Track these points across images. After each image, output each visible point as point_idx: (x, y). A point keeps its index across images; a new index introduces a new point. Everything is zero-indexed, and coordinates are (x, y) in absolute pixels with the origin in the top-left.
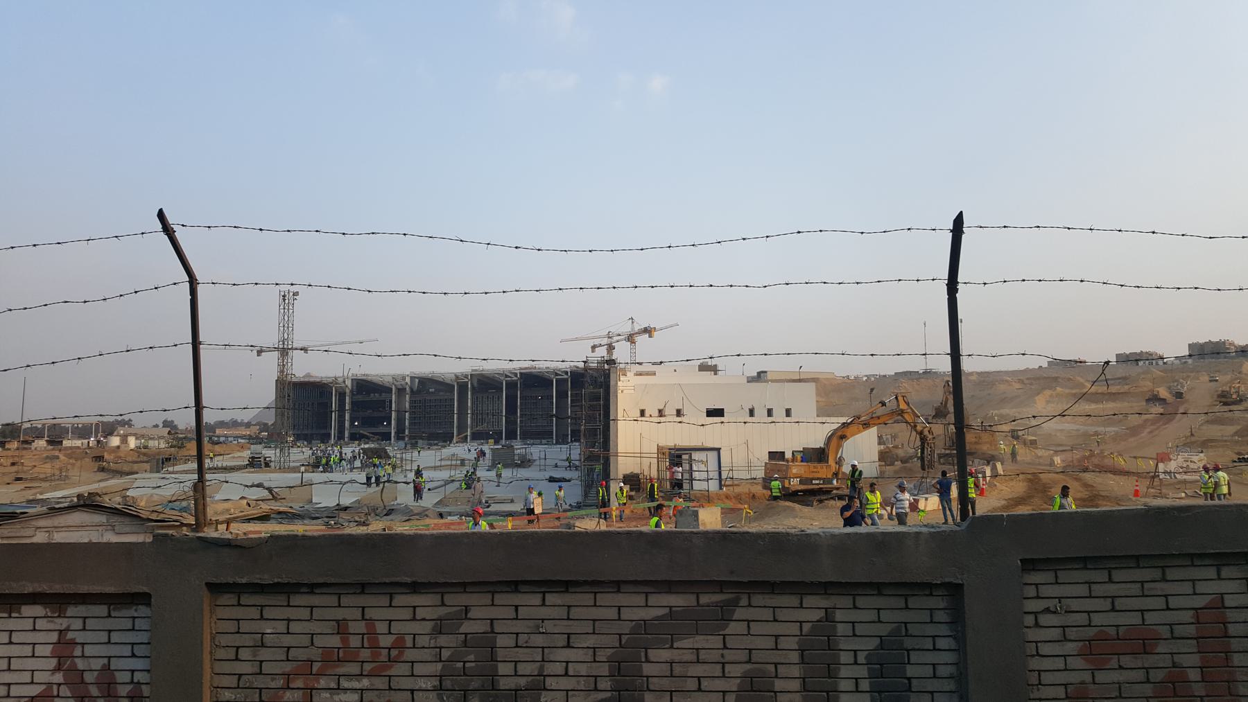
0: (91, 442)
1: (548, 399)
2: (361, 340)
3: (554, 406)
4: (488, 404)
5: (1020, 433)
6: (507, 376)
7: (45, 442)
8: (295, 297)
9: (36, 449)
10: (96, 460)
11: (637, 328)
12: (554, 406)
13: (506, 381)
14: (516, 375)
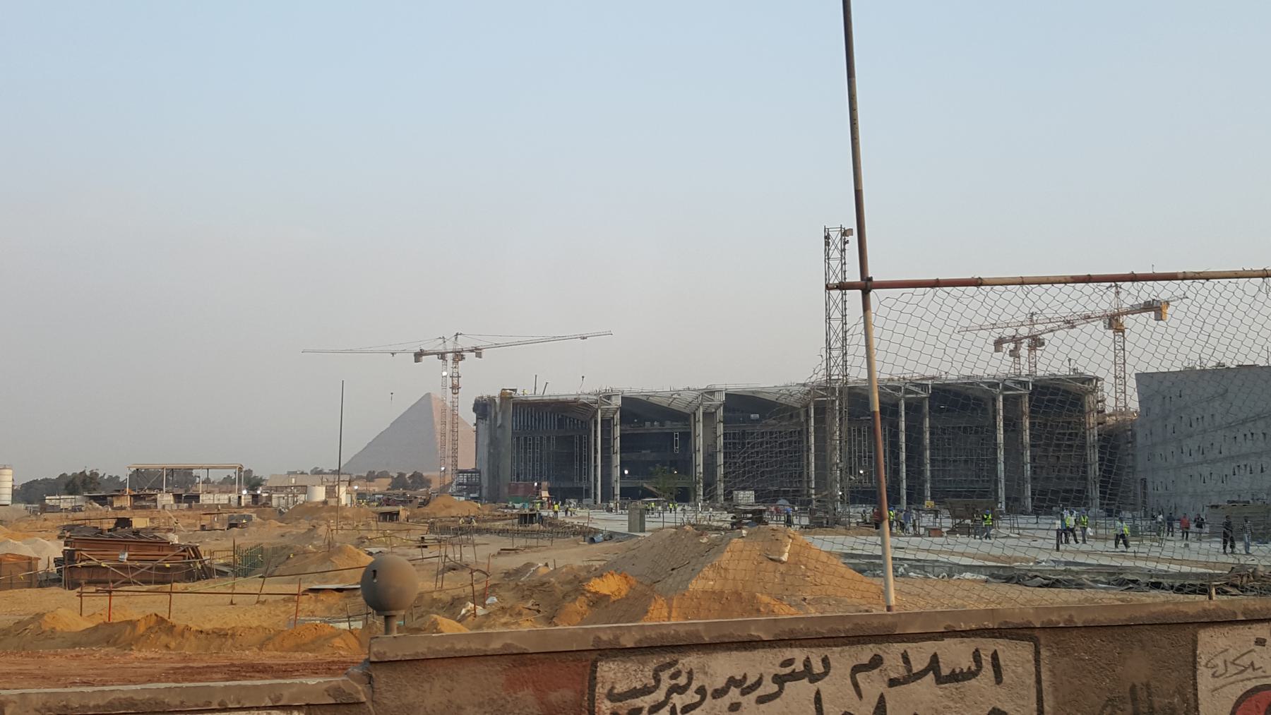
0: (243, 497)
1: (976, 432)
2: (584, 333)
5: (1104, 514)
6: (908, 391)
7: (172, 498)
9: (164, 507)
10: (385, 520)
14: (924, 387)
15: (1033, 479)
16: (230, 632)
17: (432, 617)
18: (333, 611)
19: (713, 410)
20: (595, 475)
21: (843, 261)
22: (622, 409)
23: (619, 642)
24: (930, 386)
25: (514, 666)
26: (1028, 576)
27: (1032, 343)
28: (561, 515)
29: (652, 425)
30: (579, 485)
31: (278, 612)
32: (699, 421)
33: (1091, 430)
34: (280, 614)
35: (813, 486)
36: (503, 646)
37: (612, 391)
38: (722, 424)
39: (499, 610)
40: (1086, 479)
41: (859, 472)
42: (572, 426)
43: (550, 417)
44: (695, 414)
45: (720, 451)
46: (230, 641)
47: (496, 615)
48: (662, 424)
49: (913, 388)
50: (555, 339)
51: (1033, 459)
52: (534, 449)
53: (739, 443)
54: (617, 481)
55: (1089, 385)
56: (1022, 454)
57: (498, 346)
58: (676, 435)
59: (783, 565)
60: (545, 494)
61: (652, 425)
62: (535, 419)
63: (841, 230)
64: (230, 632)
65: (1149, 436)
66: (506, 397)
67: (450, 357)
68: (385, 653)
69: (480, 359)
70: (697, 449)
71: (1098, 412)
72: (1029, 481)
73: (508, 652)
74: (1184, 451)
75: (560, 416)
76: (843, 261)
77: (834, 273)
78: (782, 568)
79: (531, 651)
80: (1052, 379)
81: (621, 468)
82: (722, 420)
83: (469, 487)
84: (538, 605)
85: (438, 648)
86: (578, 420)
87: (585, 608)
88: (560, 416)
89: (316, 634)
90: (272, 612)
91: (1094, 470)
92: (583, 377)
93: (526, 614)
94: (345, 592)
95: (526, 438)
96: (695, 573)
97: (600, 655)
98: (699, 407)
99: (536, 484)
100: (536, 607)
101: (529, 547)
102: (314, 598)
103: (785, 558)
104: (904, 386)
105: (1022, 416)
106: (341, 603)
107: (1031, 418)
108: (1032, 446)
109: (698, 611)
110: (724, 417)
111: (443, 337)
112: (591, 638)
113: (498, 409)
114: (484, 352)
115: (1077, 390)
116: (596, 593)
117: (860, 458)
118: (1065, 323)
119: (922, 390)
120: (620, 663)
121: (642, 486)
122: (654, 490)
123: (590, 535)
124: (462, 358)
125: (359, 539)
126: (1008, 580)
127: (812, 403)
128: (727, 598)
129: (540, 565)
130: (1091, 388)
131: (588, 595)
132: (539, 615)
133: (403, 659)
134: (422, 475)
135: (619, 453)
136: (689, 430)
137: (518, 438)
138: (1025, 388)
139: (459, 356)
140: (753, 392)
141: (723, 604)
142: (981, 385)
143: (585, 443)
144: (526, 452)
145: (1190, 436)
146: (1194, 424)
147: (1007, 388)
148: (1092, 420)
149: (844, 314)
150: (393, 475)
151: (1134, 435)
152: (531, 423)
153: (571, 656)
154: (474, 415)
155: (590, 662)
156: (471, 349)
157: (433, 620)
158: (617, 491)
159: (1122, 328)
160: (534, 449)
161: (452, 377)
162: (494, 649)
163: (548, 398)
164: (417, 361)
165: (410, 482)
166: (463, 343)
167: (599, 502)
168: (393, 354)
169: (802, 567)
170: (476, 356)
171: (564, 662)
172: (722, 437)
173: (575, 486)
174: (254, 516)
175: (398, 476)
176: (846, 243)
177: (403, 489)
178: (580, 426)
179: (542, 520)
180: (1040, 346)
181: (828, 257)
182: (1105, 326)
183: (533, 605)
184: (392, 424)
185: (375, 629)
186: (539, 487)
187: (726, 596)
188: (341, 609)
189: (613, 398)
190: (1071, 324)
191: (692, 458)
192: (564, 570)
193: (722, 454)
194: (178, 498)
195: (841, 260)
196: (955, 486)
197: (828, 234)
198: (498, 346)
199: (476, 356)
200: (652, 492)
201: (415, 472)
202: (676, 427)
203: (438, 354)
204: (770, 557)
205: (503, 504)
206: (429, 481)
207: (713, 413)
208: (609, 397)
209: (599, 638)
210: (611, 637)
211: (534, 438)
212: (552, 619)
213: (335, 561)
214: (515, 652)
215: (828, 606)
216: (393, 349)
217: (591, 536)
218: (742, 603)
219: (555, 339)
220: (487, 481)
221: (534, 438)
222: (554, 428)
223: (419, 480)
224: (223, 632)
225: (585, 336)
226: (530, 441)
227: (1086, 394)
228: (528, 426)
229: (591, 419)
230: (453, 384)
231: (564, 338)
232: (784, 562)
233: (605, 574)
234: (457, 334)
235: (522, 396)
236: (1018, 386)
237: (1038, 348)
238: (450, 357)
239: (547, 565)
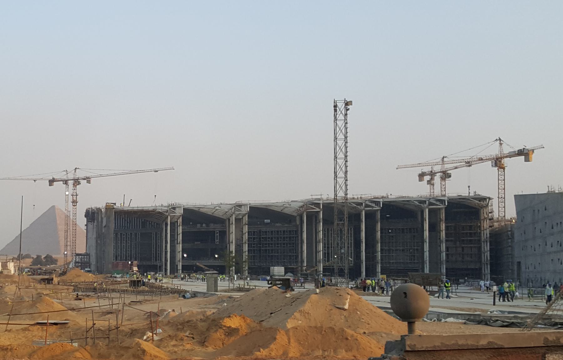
2: (156, 168)
6: (367, 206)
8: (348, 107)
11: (507, 150)
14: (377, 203)
15: (447, 261)
16: (9, 347)
17: (136, 340)
18: (54, 336)
19: (241, 217)
20: (166, 257)
21: (346, 122)
23: (560, 342)
24: (381, 203)
25: (494, 356)
26: (493, 321)
27: (443, 176)
28: (153, 281)
29: (201, 226)
30: (155, 263)
31: (20, 337)
32: (232, 223)
33: (485, 231)
34: (22, 338)
35: (305, 265)
36: (488, 343)
37: (176, 204)
38: (247, 226)
39: (168, 337)
40: (481, 262)
41: (334, 257)
42: (150, 227)
43: (137, 221)
44: (229, 220)
45: (245, 243)
46: (10, 353)
47: (167, 340)
49: (370, 204)
50: (137, 172)
51: (447, 249)
52: (126, 241)
53: (257, 238)
54: (179, 261)
55: (483, 202)
56: (440, 246)
57: (101, 176)
58: (217, 233)
59: (345, 311)
60: (135, 269)
61: (201, 226)
62: (127, 222)
63: (345, 102)
64: (9, 347)
65: (523, 234)
66: (109, 208)
67: (71, 183)
68: (415, 345)
69: (89, 184)
70: (231, 241)
71: (490, 219)
72: (444, 262)
73: (492, 347)
74: (548, 243)
75: (143, 220)
76: (346, 122)
77: (340, 129)
78: (345, 313)
79: (506, 347)
80: (460, 199)
81: (182, 253)
82: (247, 223)
83: (83, 264)
84: (193, 334)
85: (447, 343)
86: (152, 222)
87: (223, 336)
88: (143, 220)
89: (63, 349)
90: (16, 337)
92: (155, 196)
93: (186, 340)
94: (59, 325)
95: (121, 234)
96: (288, 316)
97: (547, 350)
98: (232, 215)
99: (130, 263)
100: (192, 336)
101: (146, 300)
102: (41, 329)
103: (346, 307)
104: (428, 201)
105: (440, 221)
106: (58, 332)
107: (446, 223)
108: (446, 241)
109: (307, 339)
110: (249, 221)
111: (67, 171)
112: (542, 339)
113: (103, 216)
114: (92, 180)
115: (475, 205)
116: (230, 327)
118: (467, 163)
119: (376, 205)
120: (560, 355)
121: (196, 264)
122: (203, 267)
123: (182, 294)
124: (79, 183)
125: (38, 294)
126: (479, 322)
127: (305, 213)
128: (325, 331)
129: (170, 310)
130: (486, 204)
131: (224, 328)
132: (194, 341)
133: (427, 350)
134: (52, 256)
135: (181, 243)
136: (225, 230)
137: (116, 234)
138: (442, 204)
139: (77, 182)
140: (267, 206)
141: (323, 335)
142: (414, 202)
143: (159, 237)
144: (121, 243)
145: (552, 234)
146: (555, 227)
147: (431, 204)
148: (486, 224)
149: (346, 155)
150: (33, 256)
151: (513, 234)
152: (125, 224)
153: (529, 350)
154: (86, 219)
155: (541, 355)
156: (84, 178)
157: (136, 342)
158: (180, 267)
159: (503, 166)
160: (126, 241)
161: (73, 195)
162: (482, 345)
163: (137, 209)
164: (50, 185)
165: (44, 261)
166: (80, 174)
167: (169, 274)
168: (35, 181)
169: (358, 312)
170: (87, 183)
171: (525, 354)
172: (247, 233)
173: (153, 263)
175: (37, 257)
176: (348, 110)
177: (40, 265)
178: (156, 227)
179: (144, 284)
180: (448, 178)
181: (336, 119)
182: (492, 165)
183: (189, 334)
184: (31, 225)
185: (99, 347)
186: (132, 264)
187: (324, 330)
188: (59, 336)
189: (177, 209)
190: (469, 164)
191: (227, 247)
192: (188, 314)
193: (247, 245)
195: (345, 121)
196: (395, 266)
197: (336, 104)
198: (101, 176)
199: (87, 183)
200: (202, 268)
201: (48, 255)
202: (216, 228)
203: (63, 181)
204: (336, 306)
205: (109, 275)
206: (56, 261)
207: (241, 219)
208: (174, 208)
209: (547, 339)
210: (555, 338)
211: (126, 234)
212: (204, 343)
213: (39, 307)
214: (496, 347)
215: (381, 337)
216: (35, 178)
217: (182, 294)
218: (335, 334)
219: (137, 172)
220: (95, 260)
221: (126, 234)
222: (139, 228)
223: (50, 260)
224: (5, 348)
225: (157, 170)
226: (124, 235)
227: (481, 207)
228: (123, 227)
229: (163, 222)
230: (73, 199)
231: (143, 171)
233: (231, 316)
234: (76, 169)
235: (120, 207)
236: (438, 203)
237: (447, 179)
238: (71, 183)
239: (174, 311)
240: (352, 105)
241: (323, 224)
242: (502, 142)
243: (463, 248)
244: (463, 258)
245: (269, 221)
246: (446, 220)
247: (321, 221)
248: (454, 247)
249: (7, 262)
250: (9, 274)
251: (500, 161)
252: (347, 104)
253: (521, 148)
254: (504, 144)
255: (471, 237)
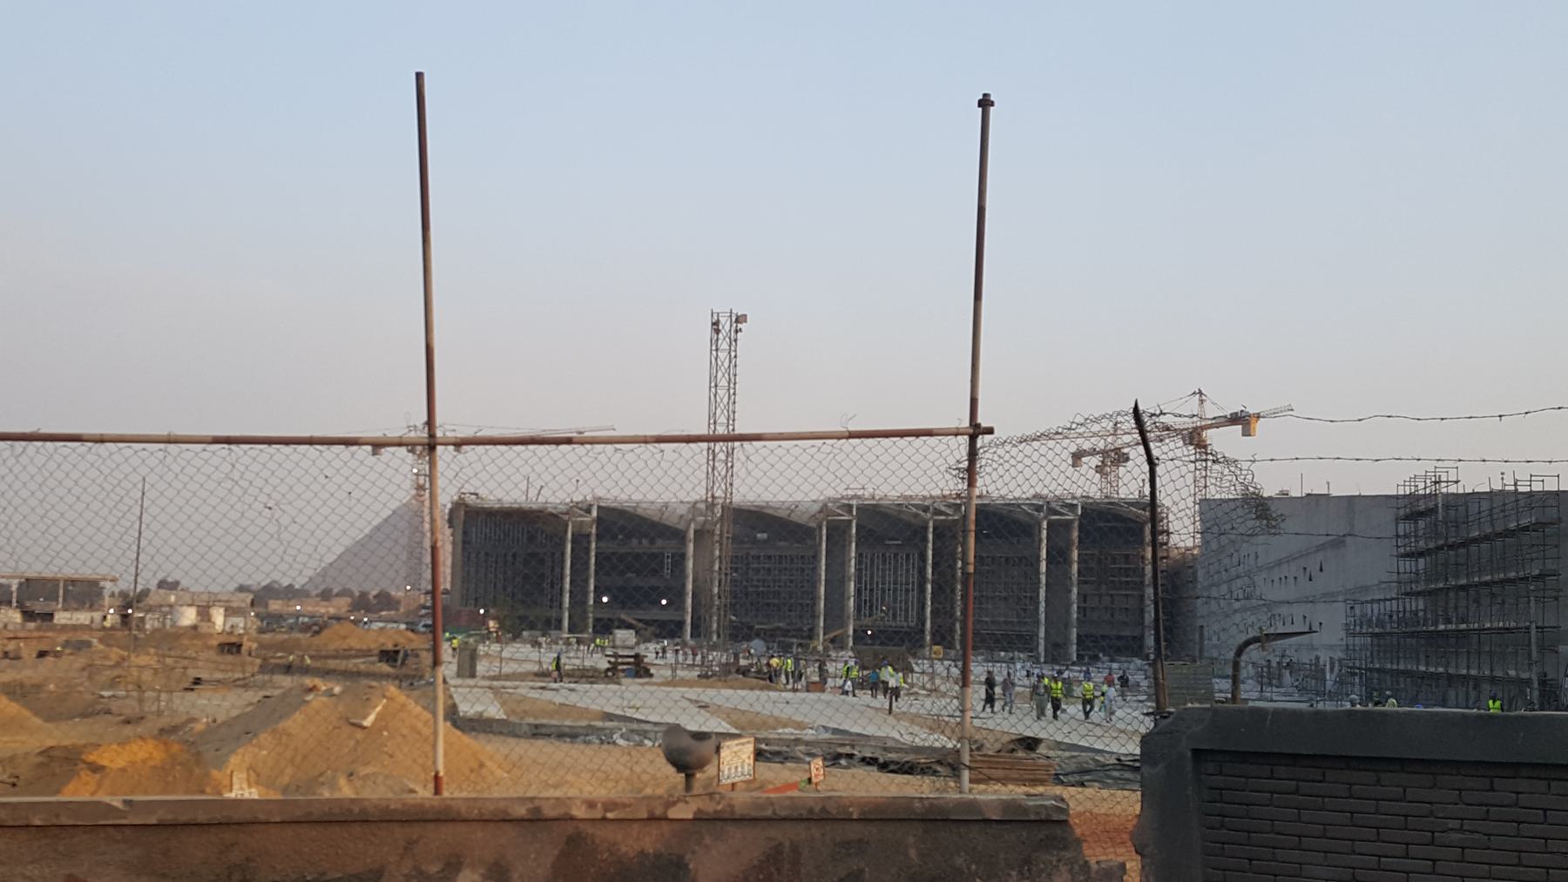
3: (568, 571)
4: (907, 571)
6: (938, 512)
8: (740, 326)
11: (1211, 412)
12: (568, 571)
13: (935, 521)
14: (1072, 507)
22: (599, 520)
40: (1142, 623)
48: (652, 541)
49: (943, 509)
51: (1083, 597)
52: (907, 571)
78: (359, 735)
91: (1149, 616)
103: (367, 722)
117: (883, 590)
127: (825, 523)
151: (1195, 573)
165: (375, 602)
174: (95, 641)
194: (28, 615)
204: (352, 721)
231: (929, 433)
232: (365, 728)
240: (746, 321)
241: (857, 545)
242: (1204, 397)
243: (1112, 595)
244: (1112, 616)
245: (765, 536)
246: (1080, 542)
247: (854, 539)
248: (1095, 595)
249: (209, 607)
250: (211, 631)
251: (1199, 434)
252: (740, 319)
253: (1237, 409)
254: (1208, 401)
255: (1128, 576)
